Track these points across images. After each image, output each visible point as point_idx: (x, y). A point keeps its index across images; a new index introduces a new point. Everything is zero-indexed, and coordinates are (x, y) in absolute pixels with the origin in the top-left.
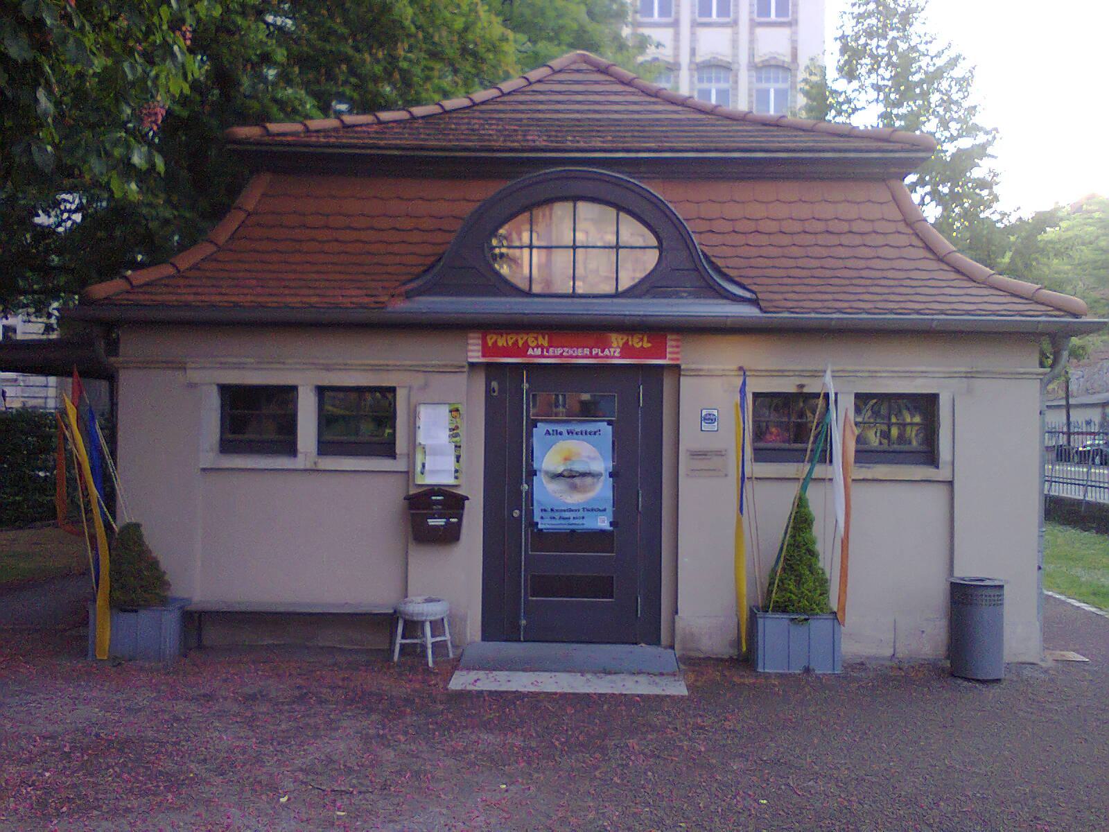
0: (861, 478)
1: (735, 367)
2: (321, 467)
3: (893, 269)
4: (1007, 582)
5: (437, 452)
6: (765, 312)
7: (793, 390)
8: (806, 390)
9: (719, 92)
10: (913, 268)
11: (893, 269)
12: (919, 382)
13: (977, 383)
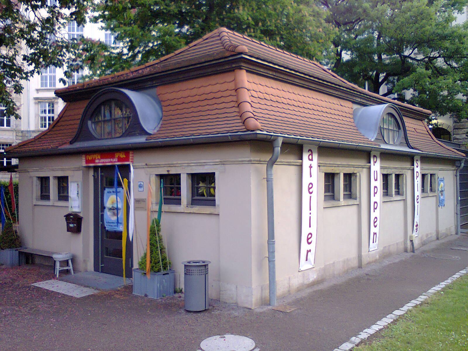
0: (189, 212)
1: (144, 164)
2: (55, 205)
3: (209, 110)
4: (210, 262)
5: (74, 200)
6: (412, 148)
7: (166, 173)
8: (171, 173)
9: (94, 10)
10: (197, 106)
11: (209, 110)
12: (206, 167)
13: (227, 166)
